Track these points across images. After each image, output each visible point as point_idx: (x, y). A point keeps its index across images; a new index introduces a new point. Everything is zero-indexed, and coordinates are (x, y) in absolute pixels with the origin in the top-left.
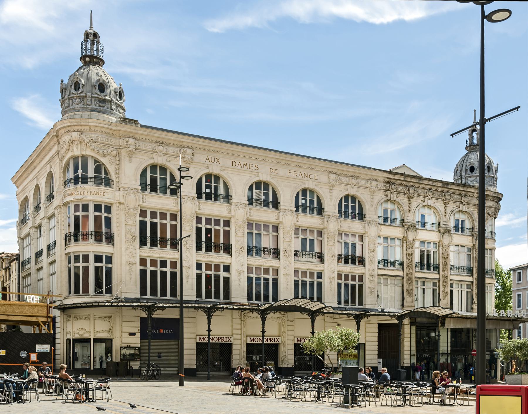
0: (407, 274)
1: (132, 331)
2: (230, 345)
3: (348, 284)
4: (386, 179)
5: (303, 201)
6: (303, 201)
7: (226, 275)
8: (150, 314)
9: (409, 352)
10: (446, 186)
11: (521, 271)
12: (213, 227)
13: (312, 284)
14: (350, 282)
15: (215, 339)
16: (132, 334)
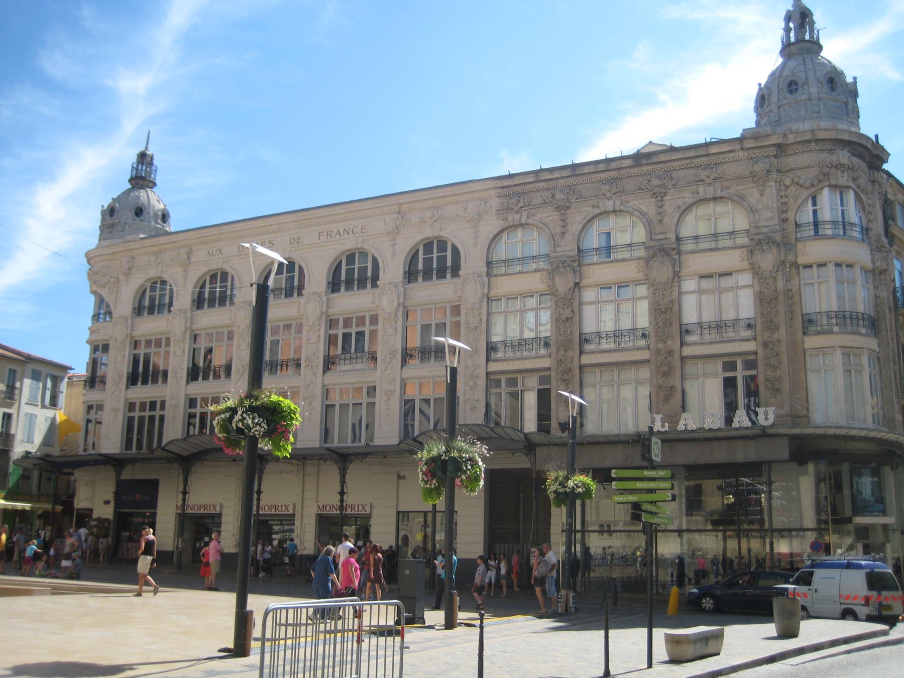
1: (107, 499)
4: (500, 190)
10: (644, 161)
15: (267, 508)
16: (107, 502)
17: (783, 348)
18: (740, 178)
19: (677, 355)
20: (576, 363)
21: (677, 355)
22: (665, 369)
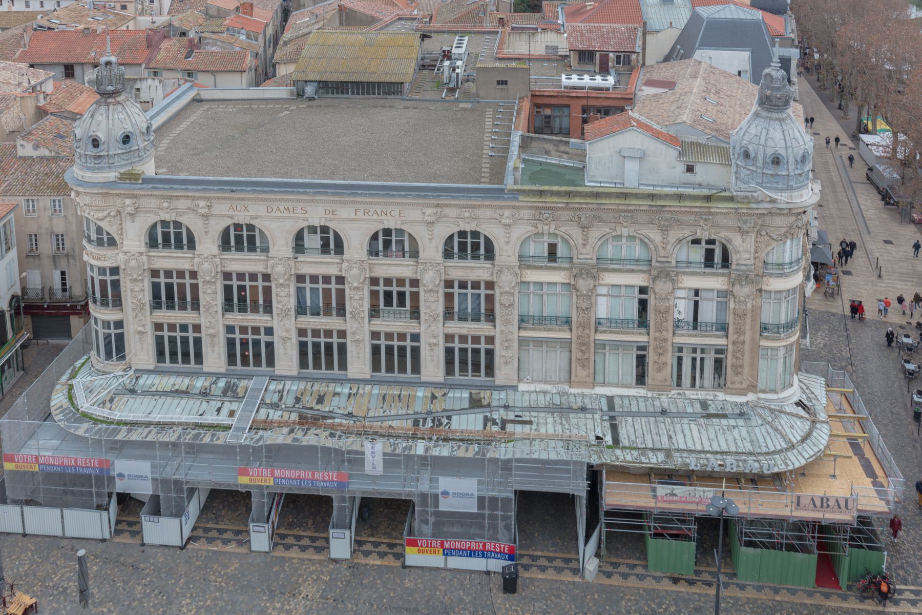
0: (578, 337)
7: (269, 339)
12: (247, 283)
17: (747, 347)
18: (729, 228)
19: (669, 343)
20: (592, 339)
21: (669, 343)
22: (660, 351)
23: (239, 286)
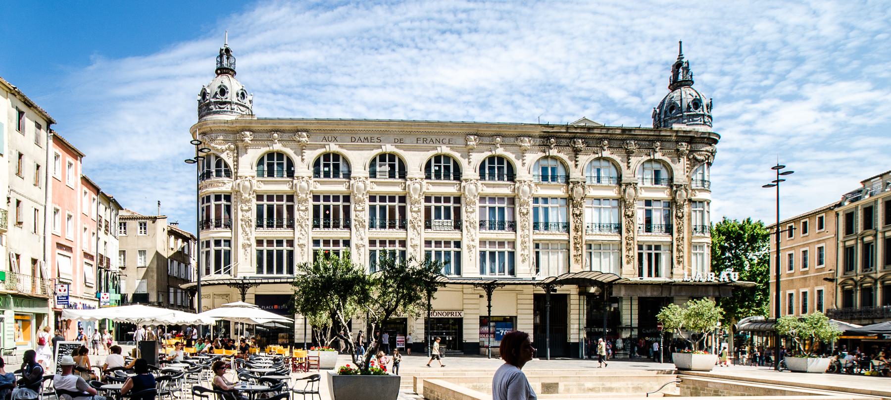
2: (461, 319)
3: (504, 252)
5: (437, 168)
6: (437, 168)
8: (548, 291)
9: (576, 326)
11: (807, 220)
13: (502, 254)
14: (388, 248)
23: (325, 206)
